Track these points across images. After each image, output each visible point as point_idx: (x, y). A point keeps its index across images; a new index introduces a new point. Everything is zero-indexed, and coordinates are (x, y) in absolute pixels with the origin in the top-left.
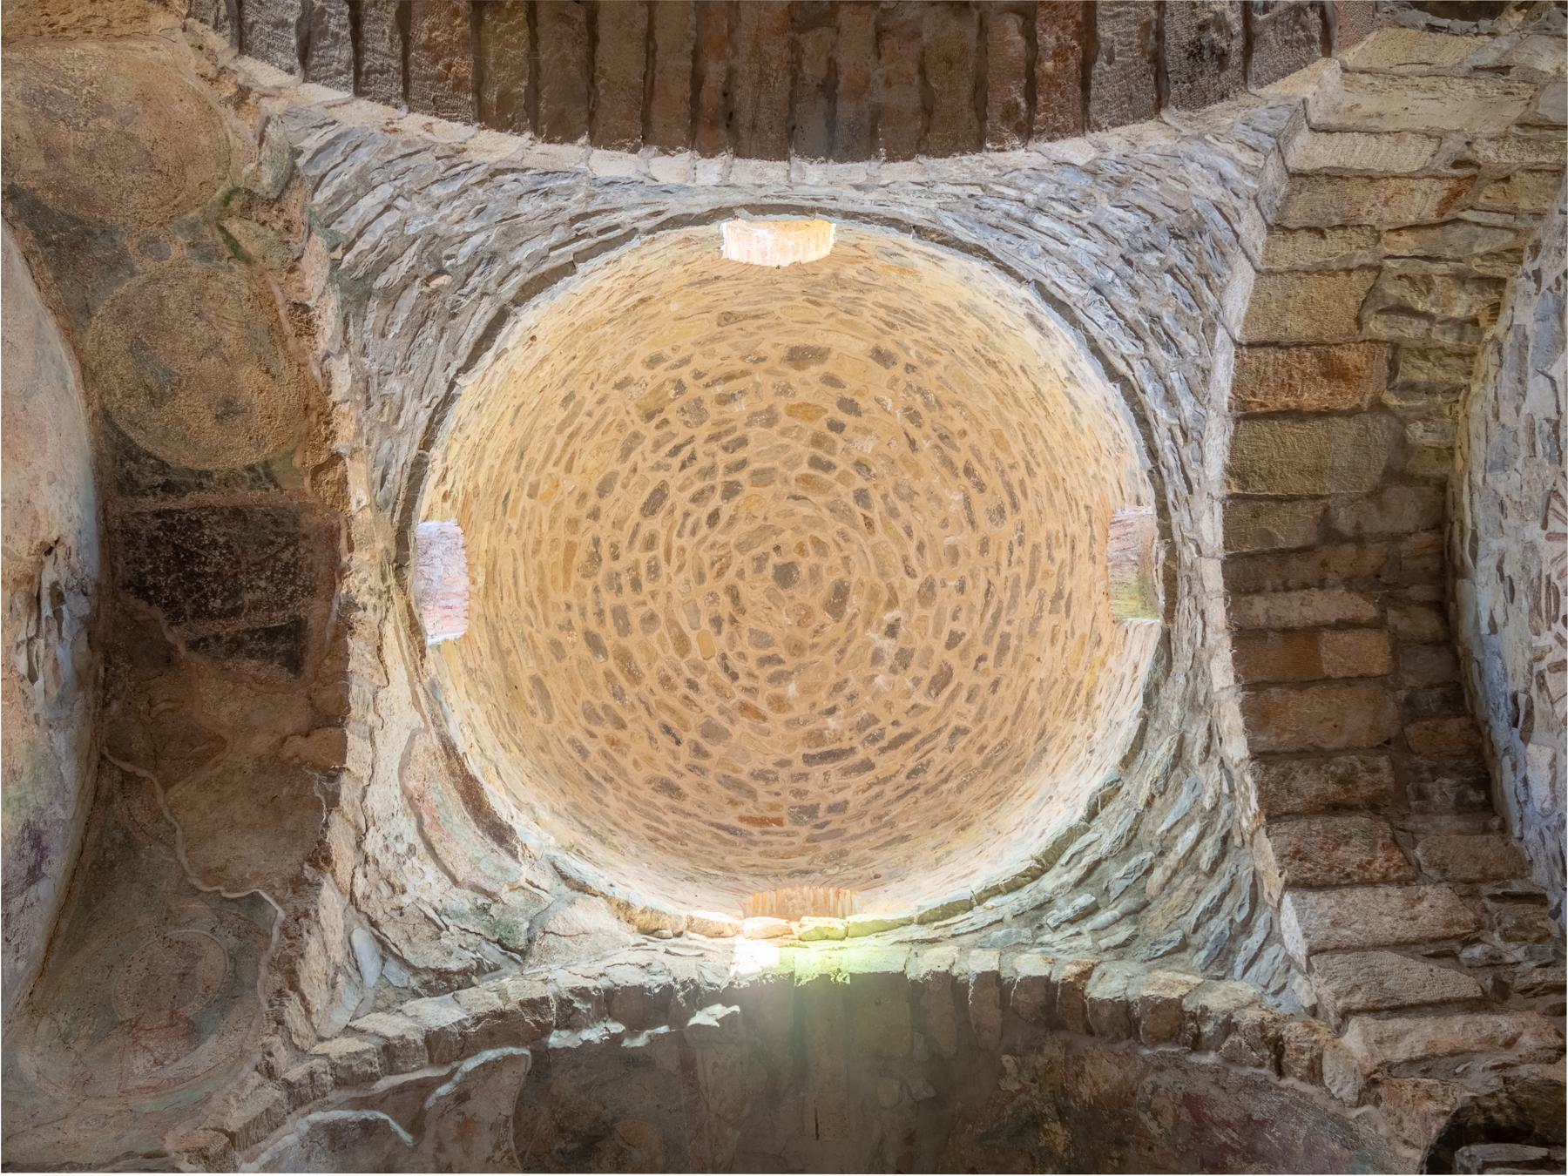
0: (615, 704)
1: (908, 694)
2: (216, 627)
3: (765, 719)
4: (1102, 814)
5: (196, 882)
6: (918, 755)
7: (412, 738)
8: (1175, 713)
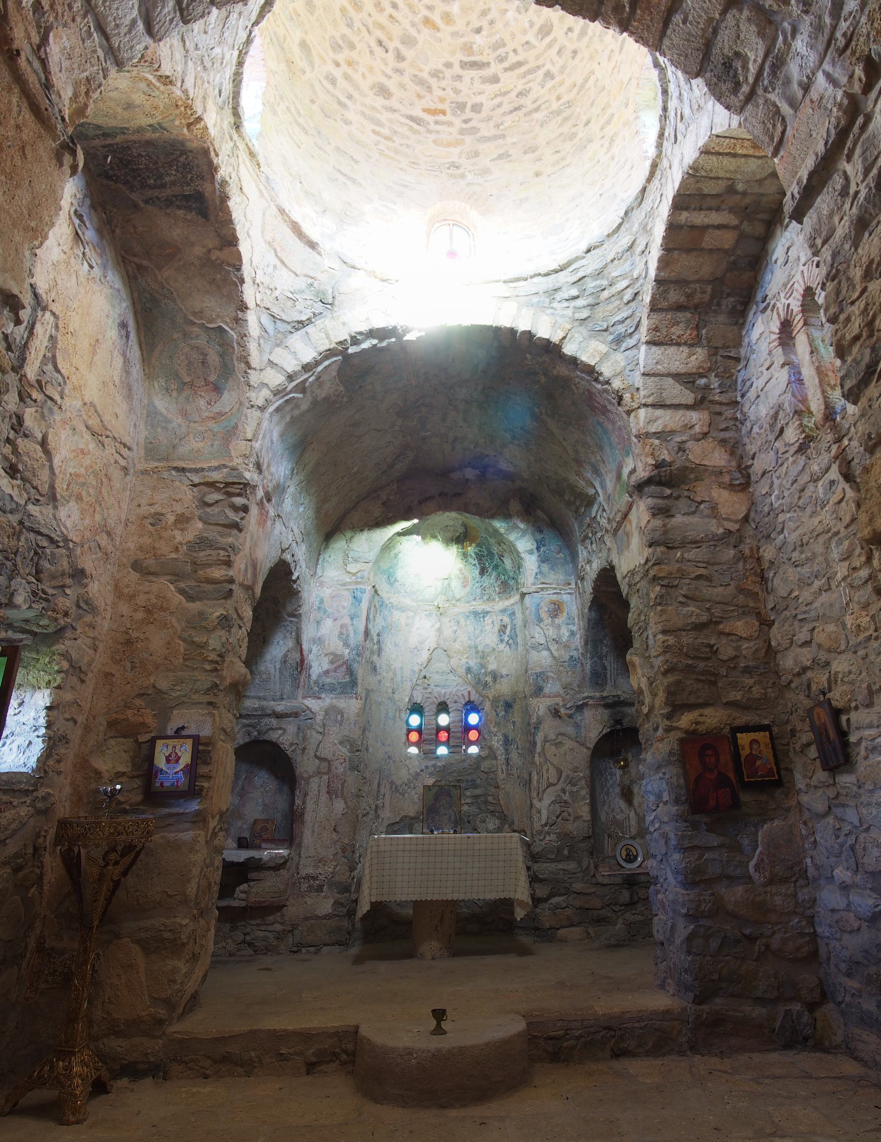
0: (348, 32)
1: (525, 32)
2: (156, 192)
3: (438, 30)
4: (592, 252)
5: (192, 318)
6: (525, 80)
7: (264, 214)
8: (636, 227)
